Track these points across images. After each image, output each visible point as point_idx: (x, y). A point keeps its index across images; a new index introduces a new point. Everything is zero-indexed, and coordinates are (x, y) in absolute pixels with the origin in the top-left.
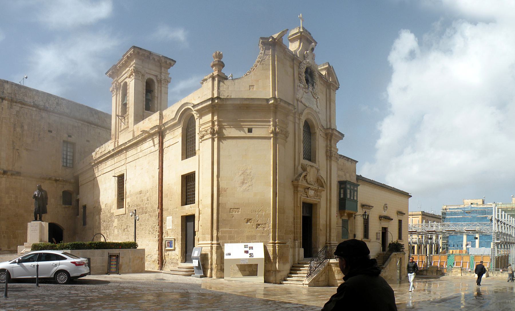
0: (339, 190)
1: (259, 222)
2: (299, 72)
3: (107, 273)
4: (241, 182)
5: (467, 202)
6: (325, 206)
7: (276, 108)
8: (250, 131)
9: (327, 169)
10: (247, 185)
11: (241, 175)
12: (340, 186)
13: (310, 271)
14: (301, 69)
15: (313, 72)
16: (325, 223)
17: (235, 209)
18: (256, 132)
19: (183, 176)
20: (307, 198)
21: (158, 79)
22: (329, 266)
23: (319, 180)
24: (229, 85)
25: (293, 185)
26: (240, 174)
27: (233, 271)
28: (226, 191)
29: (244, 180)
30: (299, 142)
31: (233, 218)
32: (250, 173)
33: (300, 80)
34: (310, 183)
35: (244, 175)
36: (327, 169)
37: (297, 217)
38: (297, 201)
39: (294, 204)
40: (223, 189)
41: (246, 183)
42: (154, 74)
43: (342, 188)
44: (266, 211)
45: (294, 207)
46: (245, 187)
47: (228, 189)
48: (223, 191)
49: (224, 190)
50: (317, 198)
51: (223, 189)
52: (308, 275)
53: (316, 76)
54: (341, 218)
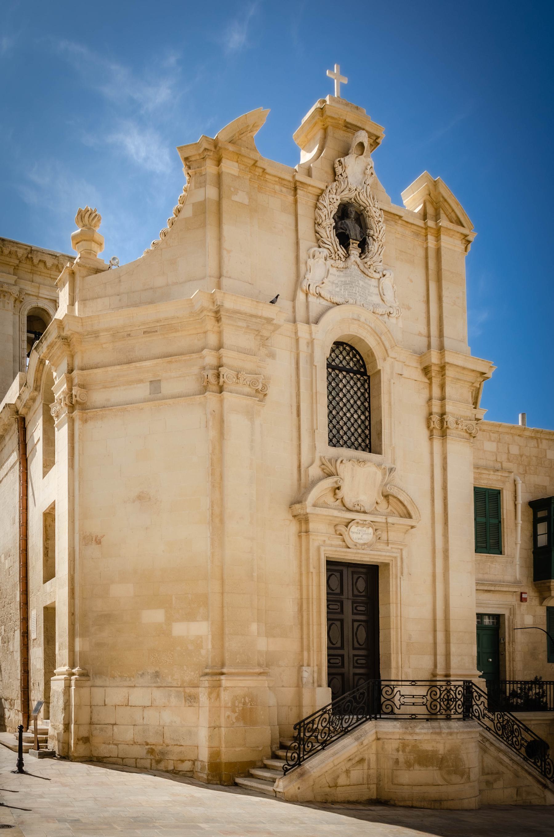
0: (530, 527)
2: (316, 219)
3: (78, 723)
5: (10, 330)
6: (429, 571)
12: (535, 515)
13: (299, 755)
14: (320, 209)
16: (427, 613)
20: (348, 550)
22: (380, 742)
23: (390, 497)
25: (294, 516)
30: (312, 403)
33: (319, 242)
34: (354, 509)
37: (308, 599)
38: (308, 559)
39: (300, 567)
43: (542, 520)
45: (301, 574)
49: (96, 540)
50: (389, 548)
52: (289, 765)
53: (373, 218)
54: (541, 603)
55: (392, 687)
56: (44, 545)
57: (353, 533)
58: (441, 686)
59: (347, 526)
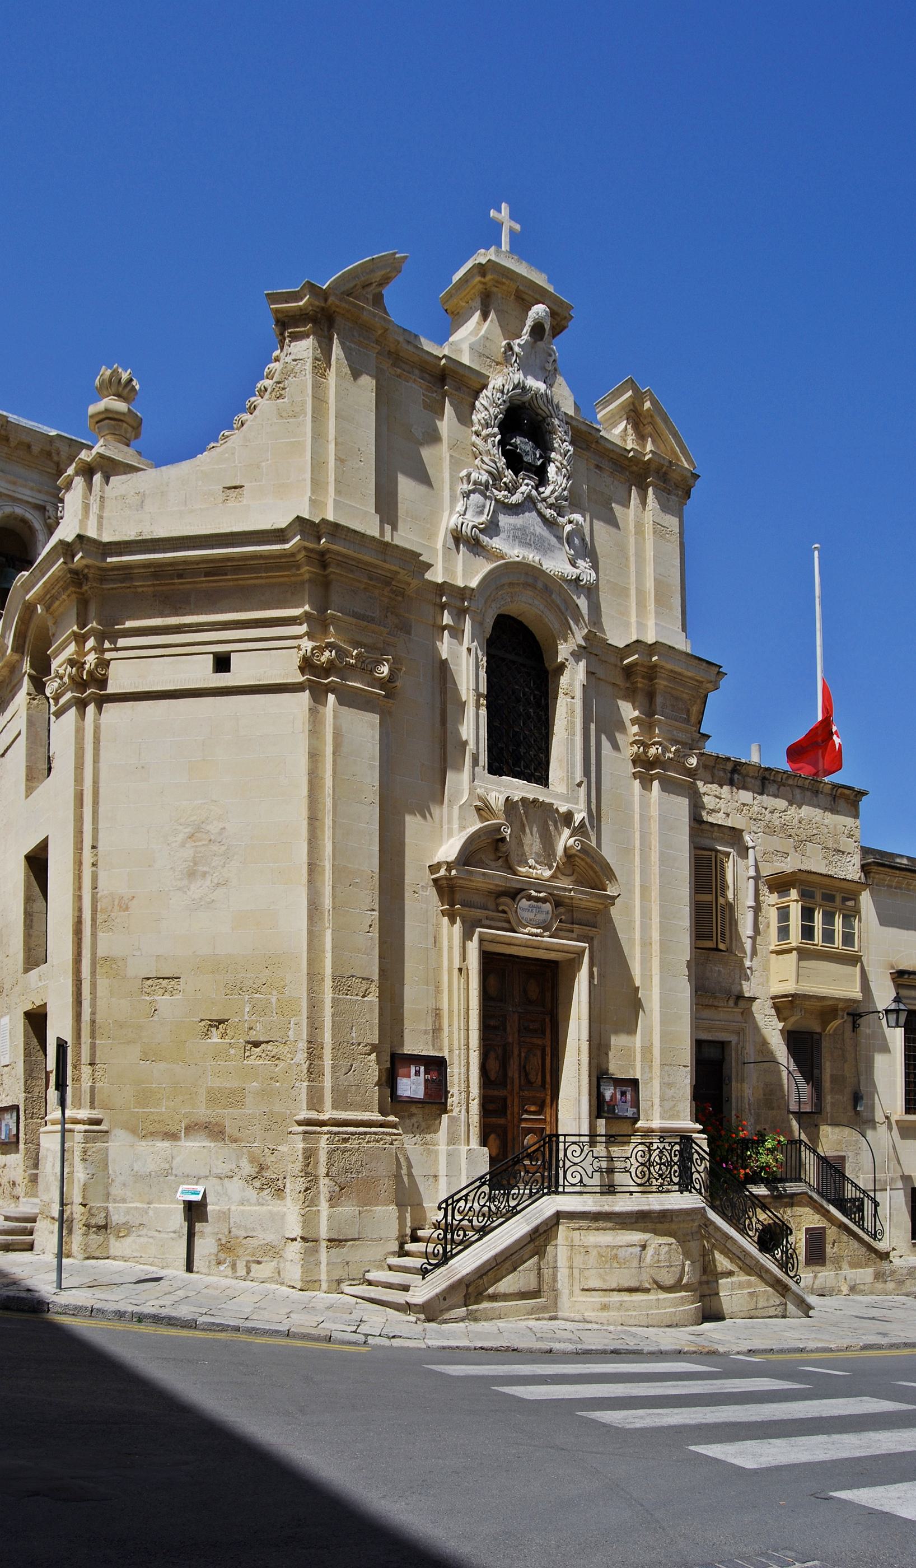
1: (254, 1036)
4: (185, 872)
7: (324, 565)
8: (222, 663)
9: (96, 760)
10: (208, 883)
11: (183, 845)
13: (445, 1249)
15: (544, 419)
17: (164, 978)
18: (241, 673)
19: (25, 856)
21: (49, 518)
24: (147, 492)
26: (180, 837)
27: (156, 1234)
28: (127, 909)
29: (195, 864)
31: (156, 1018)
32: (220, 834)
35: (194, 841)
36: (96, 760)
40: (116, 903)
41: (204, 874)
42: (30, 500)
44: (283, 987)
46: (197, 889)
47: (135, 901)
48: (116, 908)
51: (116, 903)
55: (581, 1144)
56: (25, 909)
57: (523, 909)
58: (651, 1143)
59: (513, 898)
